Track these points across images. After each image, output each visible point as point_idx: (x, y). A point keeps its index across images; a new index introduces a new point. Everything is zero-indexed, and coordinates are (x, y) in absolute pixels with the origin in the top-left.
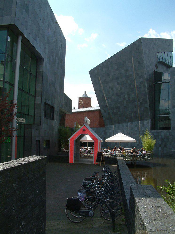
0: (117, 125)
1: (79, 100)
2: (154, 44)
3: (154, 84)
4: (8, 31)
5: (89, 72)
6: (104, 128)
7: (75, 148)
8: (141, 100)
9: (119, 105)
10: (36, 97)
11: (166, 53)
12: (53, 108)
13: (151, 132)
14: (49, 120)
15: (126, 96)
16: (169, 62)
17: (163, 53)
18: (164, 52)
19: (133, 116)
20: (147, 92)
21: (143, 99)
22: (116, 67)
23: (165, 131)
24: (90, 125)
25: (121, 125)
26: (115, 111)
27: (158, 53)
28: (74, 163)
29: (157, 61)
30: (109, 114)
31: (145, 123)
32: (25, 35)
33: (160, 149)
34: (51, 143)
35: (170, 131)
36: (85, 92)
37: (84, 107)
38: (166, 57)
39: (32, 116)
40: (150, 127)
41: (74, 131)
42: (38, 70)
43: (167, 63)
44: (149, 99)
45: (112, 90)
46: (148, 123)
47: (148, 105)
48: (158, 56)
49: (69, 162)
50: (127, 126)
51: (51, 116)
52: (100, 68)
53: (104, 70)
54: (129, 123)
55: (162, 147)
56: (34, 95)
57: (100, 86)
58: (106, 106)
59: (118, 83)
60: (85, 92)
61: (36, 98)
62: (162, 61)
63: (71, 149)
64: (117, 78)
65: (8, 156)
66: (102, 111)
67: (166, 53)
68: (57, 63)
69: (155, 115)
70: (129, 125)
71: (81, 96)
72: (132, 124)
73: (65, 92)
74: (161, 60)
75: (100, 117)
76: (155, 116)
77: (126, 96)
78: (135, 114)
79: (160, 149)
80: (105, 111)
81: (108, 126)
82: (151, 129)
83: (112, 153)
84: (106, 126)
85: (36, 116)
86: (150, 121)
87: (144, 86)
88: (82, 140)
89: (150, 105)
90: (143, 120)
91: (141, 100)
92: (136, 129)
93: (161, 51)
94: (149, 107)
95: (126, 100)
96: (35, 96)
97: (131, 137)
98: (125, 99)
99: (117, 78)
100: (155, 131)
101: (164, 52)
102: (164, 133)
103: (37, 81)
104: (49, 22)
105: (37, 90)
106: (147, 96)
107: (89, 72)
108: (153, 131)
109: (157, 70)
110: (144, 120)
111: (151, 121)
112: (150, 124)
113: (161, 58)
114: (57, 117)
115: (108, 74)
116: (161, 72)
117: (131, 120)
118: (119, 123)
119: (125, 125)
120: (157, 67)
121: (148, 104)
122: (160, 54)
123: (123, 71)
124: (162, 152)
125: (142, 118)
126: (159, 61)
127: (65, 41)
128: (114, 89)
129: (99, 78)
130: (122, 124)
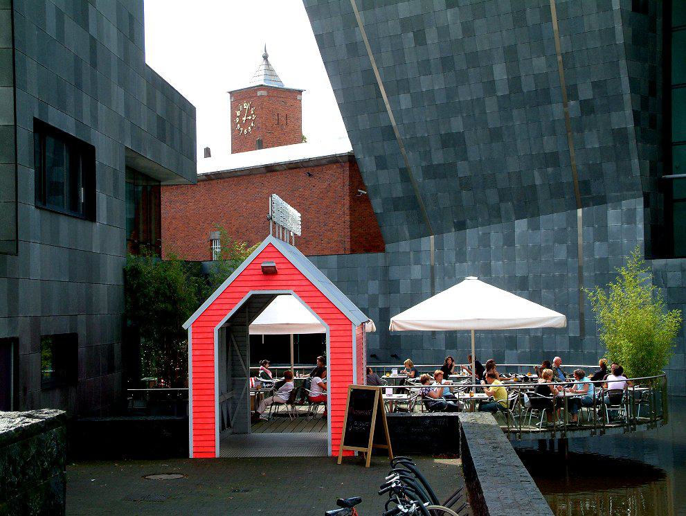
0: (450, 237)
1: (234, 107)
6: (378, 258)
8: (586, 92)
9: (457, 125)
19: (538, 182)
20: (620, 39)
25: (472, 235)
26: (438, 158)
30: (405, 175)
31: (613, 217)
34: (82, 350)
40: (641, 238)
44: (631, 80)
45: (420, 39)
46: (630, 217)
47: (624, 118)
49: (191, 455)
50: (509, 240)
54: (521, 225)
57: (350, 22)
58: (388, 132)
66: (367, 165)
70: (518, 231)
72: (535, 227)
73: (147, 62)
77: (500, 72)
78: (550, 170)
80: (381, 163)
81: (404, 246)
90: (602, 200)
91: (586, 92)
92: (561, 253)
95: (500, 94)
98: (490, 86)
100: (670, 261)
106: (623, 63)
108: (659, 263)
110: (605, 203)
112: (641, 226)
117: (528, 206)
118: (461, 226)
119: (496, 234)
121: (628, 112)
128: (432, 36)
130: (480, 230)
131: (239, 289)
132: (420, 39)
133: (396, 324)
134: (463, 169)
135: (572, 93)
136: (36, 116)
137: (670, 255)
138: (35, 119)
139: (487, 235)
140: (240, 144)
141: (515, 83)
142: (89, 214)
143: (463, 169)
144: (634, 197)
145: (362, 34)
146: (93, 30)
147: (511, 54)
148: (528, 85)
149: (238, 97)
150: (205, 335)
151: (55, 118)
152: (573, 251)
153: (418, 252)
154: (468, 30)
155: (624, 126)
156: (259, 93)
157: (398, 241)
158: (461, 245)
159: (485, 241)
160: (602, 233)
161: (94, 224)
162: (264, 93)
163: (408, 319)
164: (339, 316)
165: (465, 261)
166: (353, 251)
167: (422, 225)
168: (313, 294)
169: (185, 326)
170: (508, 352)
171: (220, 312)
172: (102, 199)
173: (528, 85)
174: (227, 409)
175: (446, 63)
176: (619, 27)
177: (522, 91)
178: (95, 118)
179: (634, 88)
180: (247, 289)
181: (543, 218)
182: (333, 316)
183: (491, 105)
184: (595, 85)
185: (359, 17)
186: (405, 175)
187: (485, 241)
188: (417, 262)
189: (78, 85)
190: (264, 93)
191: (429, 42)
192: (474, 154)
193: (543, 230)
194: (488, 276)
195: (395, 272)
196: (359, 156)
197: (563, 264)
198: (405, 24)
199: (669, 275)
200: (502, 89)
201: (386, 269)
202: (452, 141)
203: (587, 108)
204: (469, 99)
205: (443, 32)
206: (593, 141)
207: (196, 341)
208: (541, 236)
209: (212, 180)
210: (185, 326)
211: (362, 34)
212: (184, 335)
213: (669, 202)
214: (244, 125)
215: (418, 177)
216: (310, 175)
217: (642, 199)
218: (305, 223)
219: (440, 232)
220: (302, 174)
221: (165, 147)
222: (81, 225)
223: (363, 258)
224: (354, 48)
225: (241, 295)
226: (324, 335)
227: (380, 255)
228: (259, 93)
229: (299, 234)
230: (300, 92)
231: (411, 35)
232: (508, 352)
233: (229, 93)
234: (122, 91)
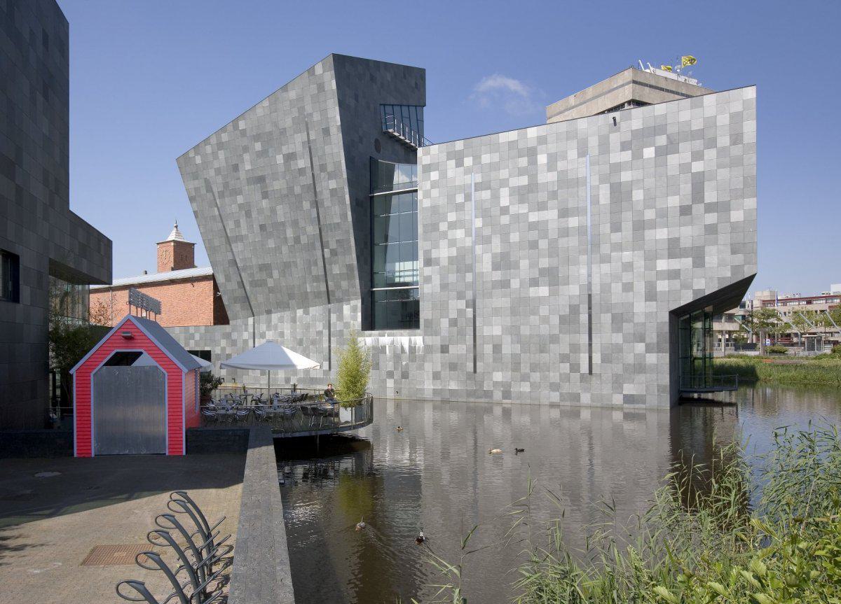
2: (372, 79)
7: (94, 402)
11: (405, 109)
19: (308, 290)
21: (338, 241)
26: (257, 277)
27: (382, 107)
31: (346, 309)
41: (711, 333)
46: (354, 310)
49: (75, 455)
50: (294, 320)
54: (300, 312)
55: (395, 377)
63: (79, 404)
67: (405, 109)
70: (298, 315)
72: (306, 313)
73: (74, 207)
75: (215, 294)
78: (315, 284)
79: (390, 383)
80: (228, 278)
81: (239, 322)
83: (794, 323)
86: (358, 303)
90: (340, 301)
93: (392, 101)
97: (284, 352)
101: (401, 106)
111: (362, 303)
118: (269, 312)
119: (287, 314)
121: (354, 256)
130: (279, 315)
131: (108, 349)
136: (52, 257)
143: (270, 283)
158: (269, 322)
161: (17, 305)
164: (174, 366)
165: (271, 330)
169: (71, 372)
180: (113, 348)
182: (170, 367)
183: (285, 249)
184: (338, 241)
191: (253, 216)
195: (235, 336)
204: (387, 459)
205: (260, 211)
207: (78, 382)
208: (308, 319)
210: (71, 372)
212: (72, 376)
221: (85, 261)
230: (194, 244)
231: (244, 212)
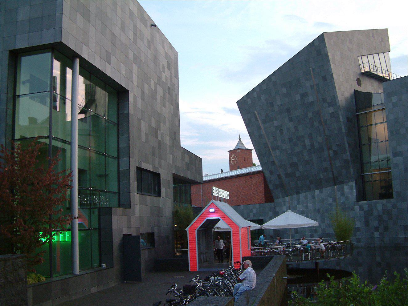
0: (295, 197)
1: (230, 156)
3: (358, 115)
4: (52, 53)
5: (238, 103)
6: (272, 204)
8: (335, 148)
9: (295, 160)
10: (120, 159)
12: (158, 175)
13: (358, 205)
14: (148, 198)
15: (307, 142)
16: (380, 70)
17: (370, 57)
18: (378, 53)
19: (322, 177)
20: (344, 131)
22: (284, 91)
23: (384, 201)
24: (229, 202)
25: (302, 195)
26: (289, 171)
27: (360, 58)
28: (198, 270)
29: (359, 72)
30: (279, 176)
31: (346, 188)
32: (85, 56)
33: (377, 235)
34: (156, 237)
35: (392, 200)
36: (240, 139)
37: (238, 168)
38: (378, 64)
39: (115, 193)
40: (355, 195)
42: (120, 112)
43: (380, 74)
44: (348, 143)
45: (281, 132)
46: (351, 188)
47: (347, 156)
48: (361, 63)
49: (190, 270)
50: (314, 197)
51: (155, 189)
52: (255, 94)
53: (263, 97)
54: (317, 192)
55: (380, 231)
56: (116, 155)
57: (259, 128)
58: (273, 163)
59: (291, 120)
60: (240, 139)
61: (120, 161)
62: (367, 72)
64: (288, 110)
65: (386, 271)
66: (267, 174)
68: (161, 96)
69: (363, 172)
71: (233, 148)
74: (367, 69)
76: (364, 175)
77: (307, 142)
78: (325, 173)
79: (377, 235)
80: (271, 173)
81: (280, 200)
82: (357, 199)
84: (275, 200)
85: (121, 192)
86: (353, 184)
87: (338, 120)
88: (218, 228)
89: (350, 154)
90: (342, 183)
91: (335, 148)
92: (330, 200)
94: (349, 158)
95: (308, 149)
96: (118, 158)
98: (305, 147)
99: (288, 110)
100: (364, 202)
101: (378, 53)
102: (380, 205)
103: (120, 132)
104: (135, 26)
105: (120, 146)
106: (345, 138)
107: (238, 103)
108: (361, 203)
109: (361, 89)
110: (343, 183)
111: (356, 183)
112: (355, 191)
113: (366, 65)
114: (167, 191)
115: (272, 105)
116: (369, 92)
117: (319, 185)
118: (298, 193)
119: (309, 194)
120: (359, 83)
121: (348, 154)
122: (365, 58)
123: (298, 97)
124: (381, 240)
125: (336, 181)
126: (363, 71)
127: (176, 54)
128: (285, 131)
129: (255, 113)
130: (304, 194)
132: (281, 132)
133: (263, 227)
134: (298, 174)
135: (330, 148)
137: (366, 200)
138: (137, 167)
139: (306, 195)
140: (232, 168)
141: (312, 146)
142: (159, 195)
143: (298, 174)
144: (352, 181)
145: (263, 132)
146: (159, 138)
147: (310, 137)
148: (316, 146)
149: (231, 152)
150: (193, 232)
151: (144, 166)
152: (335, 199)
153: (284, 202)
154: (296, 129)
155: (347, 158)
156: (238, 151)
157: (278, 199)
158: (298, 199)
159: (306, 197)
160: (343, 194)
162: (239, 151)
163: (268, 225)
166: (266, 202)
167: (286, 193)
168: (226, 218)
169: (186, 229)
170: (315, 234)
171: (197, 225)
172: (163, 190)
173: (316, 146)
174: (203, 257)
175: (290, 140)
176: (343, 127)
177: (315, 148)
178: (160, 166)
179: (349, 145)
181: (324, 189)
185: (262, 126)
186: (279, 176)
187: (306, 197)
188: (285, 205)
189: (154, 155)
190: (239, 151)
191: (284, 133)
192: (301, 168)
193: (324, 193)
194: (294, 210)
196: (264, 171)
197: (331, 204)
198: (276, 128)
199: (364, 206)
200: (308, 148)
201: (275, 208)
202: (294, 165)
203: (335, 152)
206: (338, 163)
209: (220, 180)
210: (186, 229)
211: (263, 132)
213: (364, 182)
214: (233, 161)
215: (283, 176)
216: (251, 178)
217: (354, 182)
218: (230, 195)
219: (291, 195)
220: (248, 177)
222: (155, 198)
223: (267, 205)
224: (260, 136)
225: (201, 221)
226: (230, 232)
227: (272, 203)
228: (238, 151)
229: (228, 199)
231: (278, 131)
232: (315, 234)
233: (228, 151)
234: (171, 156)
